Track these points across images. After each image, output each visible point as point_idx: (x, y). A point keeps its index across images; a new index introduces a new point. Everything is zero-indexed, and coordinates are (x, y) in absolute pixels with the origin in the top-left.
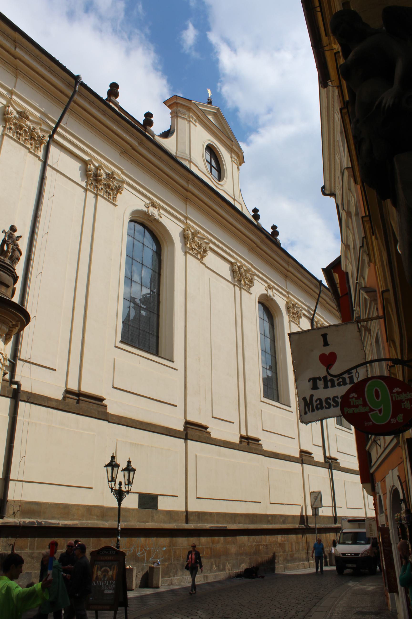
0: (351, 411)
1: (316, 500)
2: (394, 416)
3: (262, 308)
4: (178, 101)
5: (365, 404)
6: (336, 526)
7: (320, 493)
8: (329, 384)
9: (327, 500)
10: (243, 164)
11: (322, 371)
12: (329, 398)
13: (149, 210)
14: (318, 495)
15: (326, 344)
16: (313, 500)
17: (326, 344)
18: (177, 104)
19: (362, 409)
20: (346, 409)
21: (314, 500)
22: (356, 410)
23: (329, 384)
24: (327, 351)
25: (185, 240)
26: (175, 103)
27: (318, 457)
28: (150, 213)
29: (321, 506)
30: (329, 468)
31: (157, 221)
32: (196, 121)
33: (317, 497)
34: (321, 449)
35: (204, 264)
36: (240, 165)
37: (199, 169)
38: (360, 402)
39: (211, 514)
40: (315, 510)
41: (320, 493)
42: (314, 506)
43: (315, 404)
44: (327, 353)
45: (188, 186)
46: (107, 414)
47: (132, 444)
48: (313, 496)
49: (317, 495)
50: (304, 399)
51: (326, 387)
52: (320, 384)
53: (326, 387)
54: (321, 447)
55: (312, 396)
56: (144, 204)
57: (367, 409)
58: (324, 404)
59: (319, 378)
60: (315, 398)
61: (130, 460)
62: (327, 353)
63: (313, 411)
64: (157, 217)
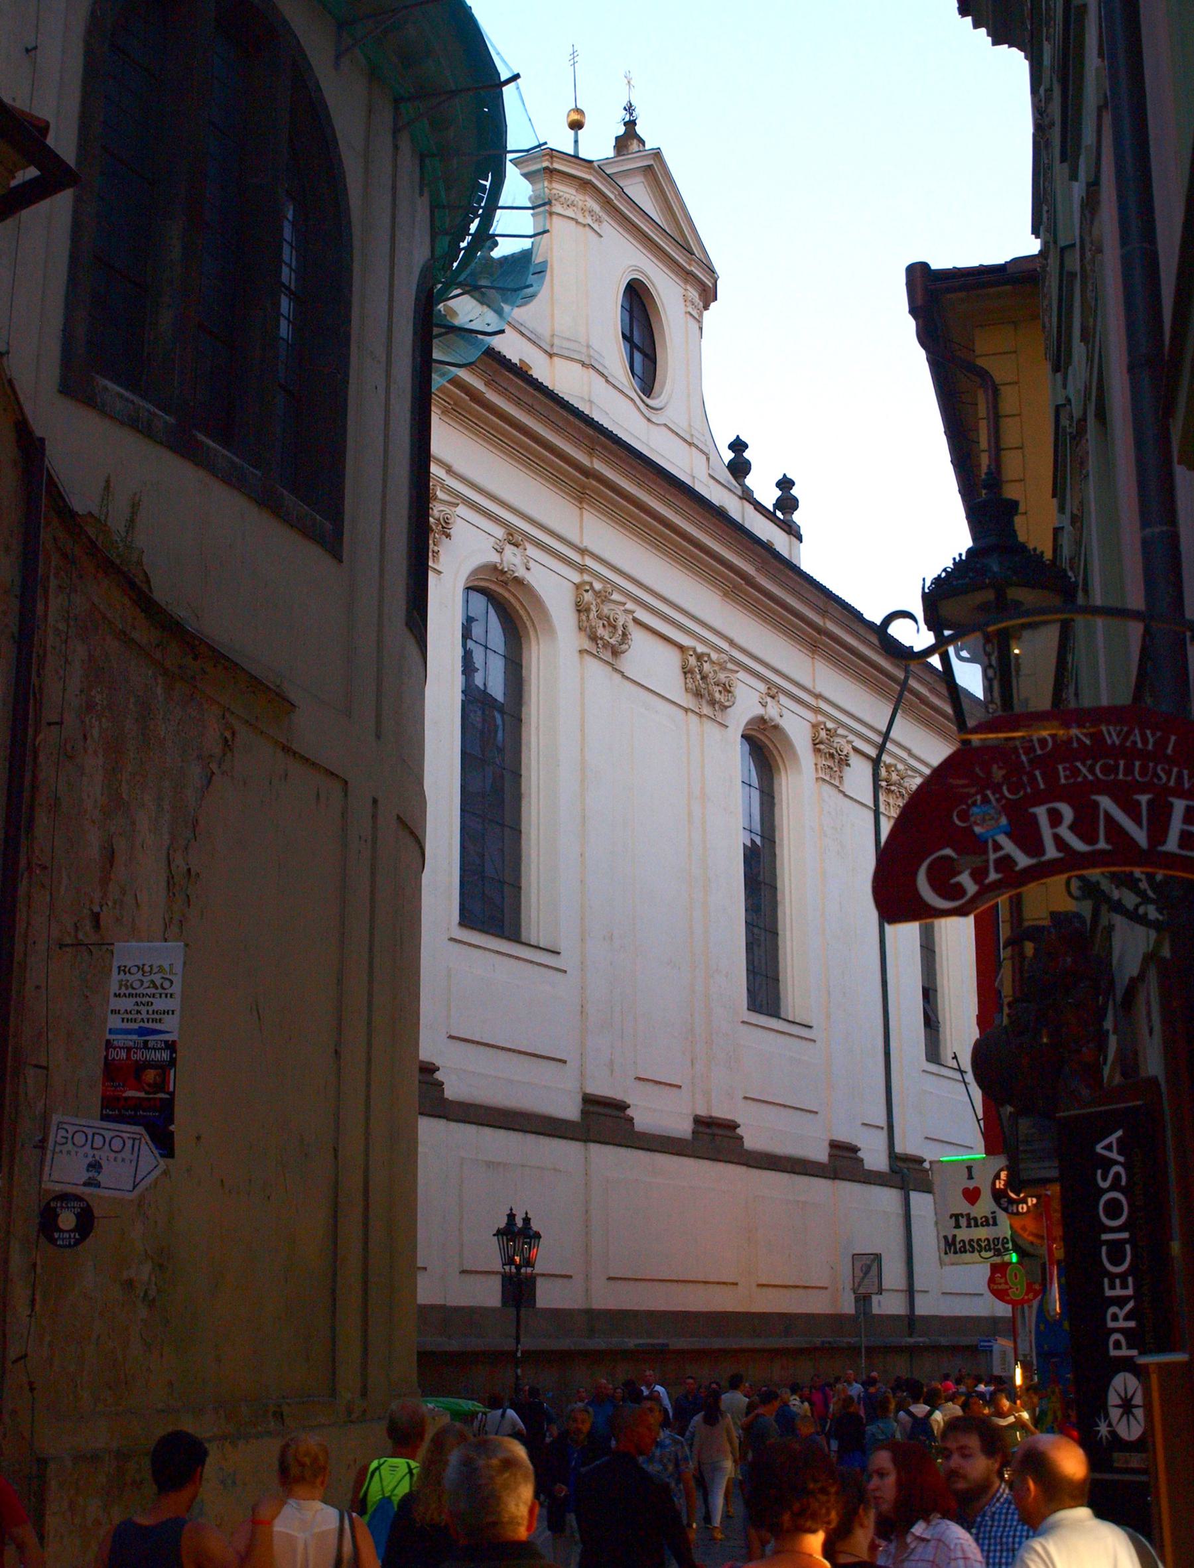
0: (995, 1287)
1: (866, 1273)
2: (1027, 1294)
3: (747, 747)
4: (556, 166)
5: (1006, 1283)
6: (911, 1340)
7: (878, 1257)
8: (972, 1223)
9: (893, 1274)
10: (713, 305)
11: (963, 1207)
12: (972, 1240)
13: (504, 559)
14: (873, 1261)
15: (970, 1177)
16: (859, 1274)
17: (970, 1177)
18: (550, 172)
19: (1003, 1287)
20: (992, 1285)
21: (862, 1275)
22: (1000, 1287)
23: (972, 1223)
24: (971, 1185)
25: (579, 616)
26: (546, 168)
27: (875, 1158)
28: (505, 564)
29: (880, 1291)
30: (902, 1188)
31: (519, 582)
32: (599, 220)
33: (869, 1267)
34: (883, 1135)
35: (622, 673)
36: (706, 307)
37: (607, 381)
38: (1003, 1280)
39: (634, 1314)
40: (863, 1300)
41: (878, 1257)
42: (862, 1290)
43: (958, 1246)
44: (971, 1188)
45: (592, 462)
46: (444, 1101)
47: (489, 1164)
48: (858, 1264)
49: (868, 1262)
50: (945, 1237)
51: (969, 1226)
52: (963, 1222)
53: (969, 1226)
54: (882, 1128)
55: (954, 1236)
56: (492, 544)
57: (1007, 1287)
58: (968, 1247)
59: (962, 1215)
60: (958, 1239)
61: (514, 1212)
62: (971, 1188)
63: (955, 1253)
64: (520, 572)
